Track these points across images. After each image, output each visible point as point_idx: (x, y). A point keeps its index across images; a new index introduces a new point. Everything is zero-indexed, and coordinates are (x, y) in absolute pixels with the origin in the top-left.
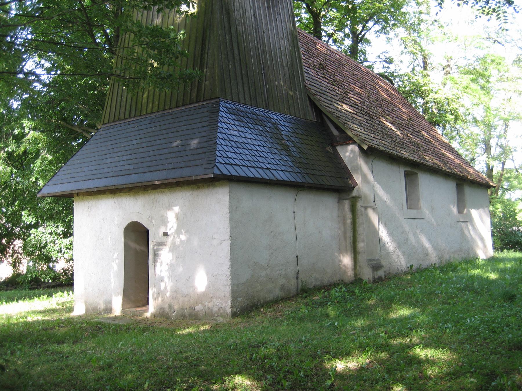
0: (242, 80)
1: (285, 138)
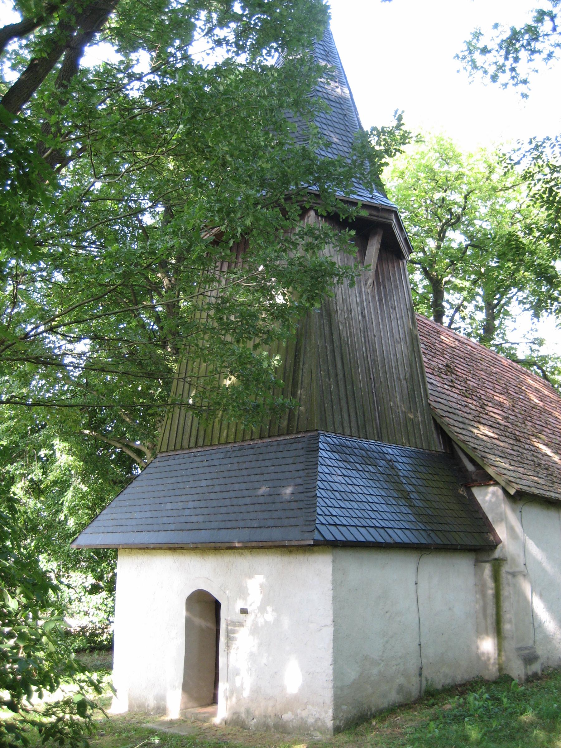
0: (347, 403)
1: (404, 481)
